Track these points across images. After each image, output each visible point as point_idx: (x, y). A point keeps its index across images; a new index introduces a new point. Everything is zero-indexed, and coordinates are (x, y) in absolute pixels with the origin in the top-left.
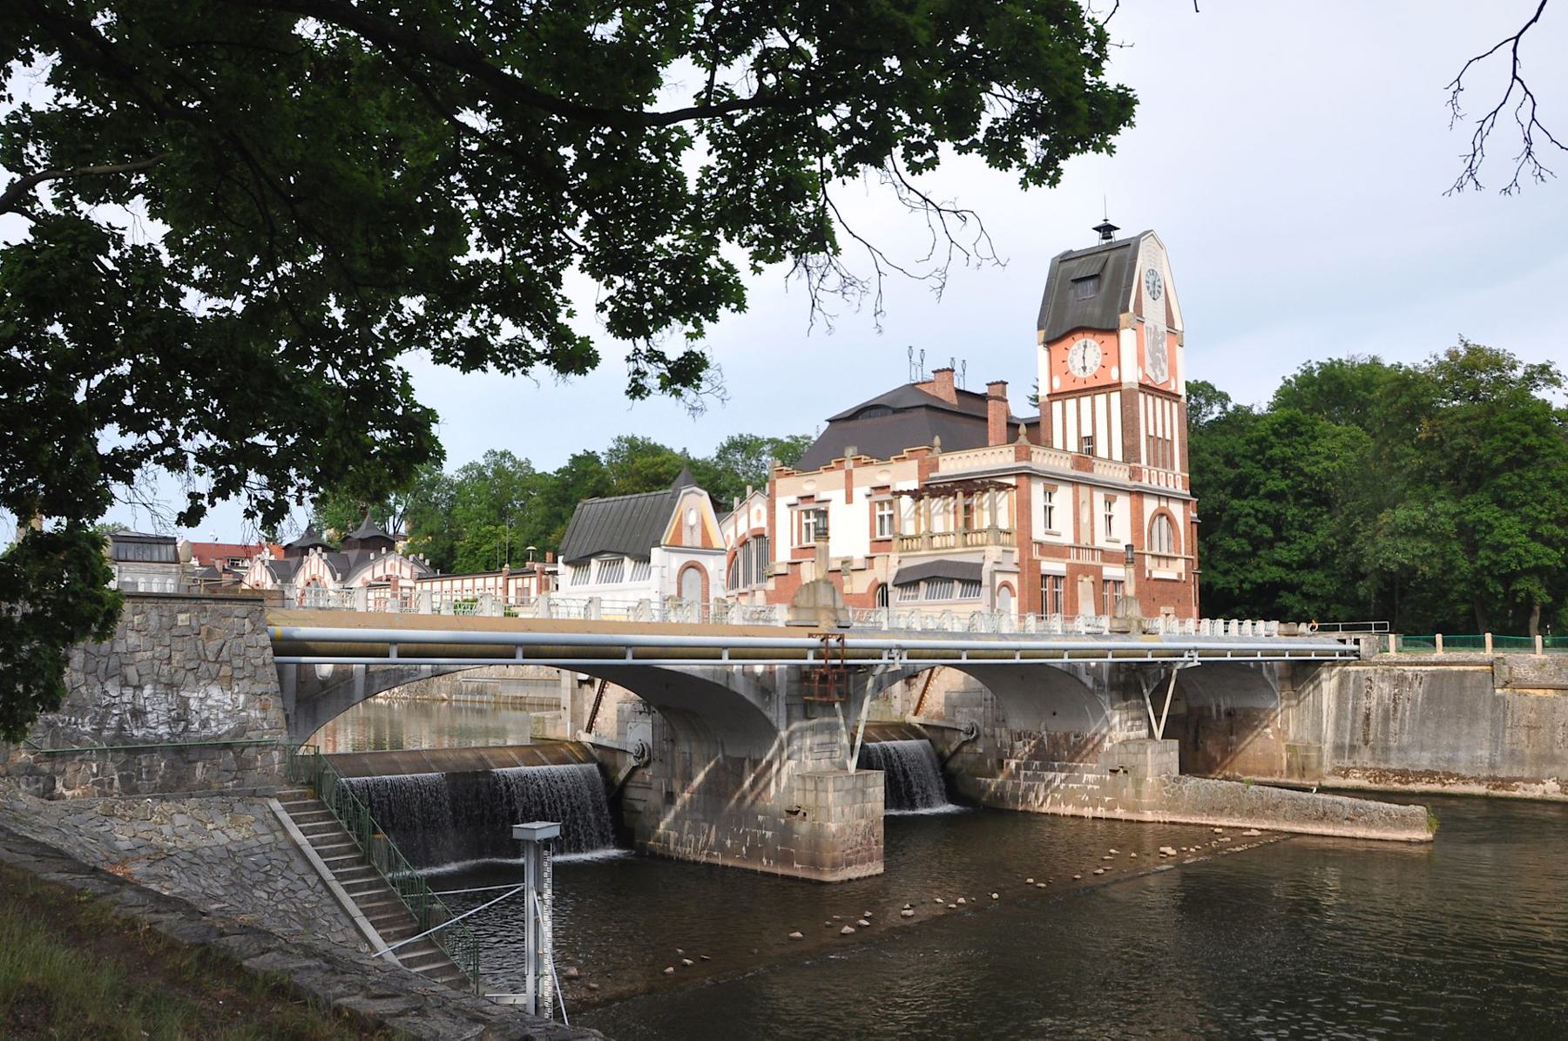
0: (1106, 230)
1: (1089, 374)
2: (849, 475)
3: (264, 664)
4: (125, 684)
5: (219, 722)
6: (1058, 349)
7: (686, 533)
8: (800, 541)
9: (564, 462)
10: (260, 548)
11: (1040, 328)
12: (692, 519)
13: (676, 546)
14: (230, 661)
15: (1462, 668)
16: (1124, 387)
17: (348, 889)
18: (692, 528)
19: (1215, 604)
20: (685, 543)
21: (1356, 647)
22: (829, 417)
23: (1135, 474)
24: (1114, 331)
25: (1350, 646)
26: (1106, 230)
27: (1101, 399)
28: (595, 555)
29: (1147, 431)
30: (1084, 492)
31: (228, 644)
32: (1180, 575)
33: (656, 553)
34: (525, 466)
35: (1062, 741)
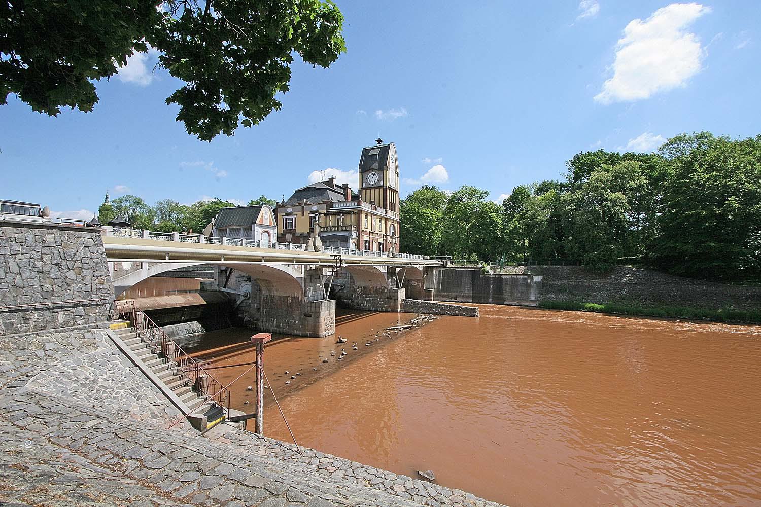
0: (379, 141)
2: (303, 207)
3: (101, 262)
6: (364, 175)
8: (286, 228)
17: (172, 389)
19: (403, 250)
26: (379, 141)
27: (377, 190)
31: (79, 251)
34: (177, 205)
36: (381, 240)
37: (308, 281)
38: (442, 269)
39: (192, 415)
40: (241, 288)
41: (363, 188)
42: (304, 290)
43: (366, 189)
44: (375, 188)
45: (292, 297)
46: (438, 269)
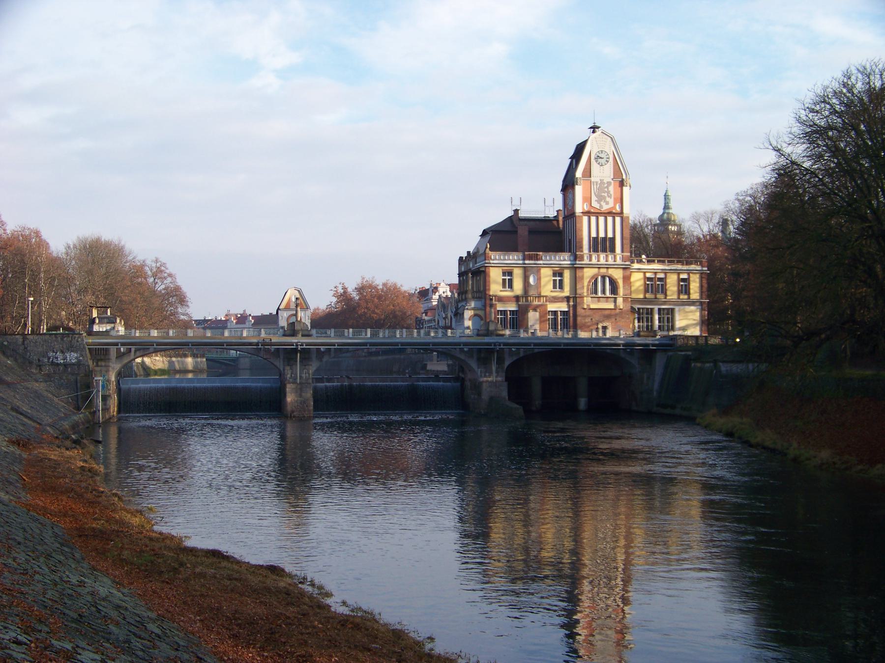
4: (54, 352)
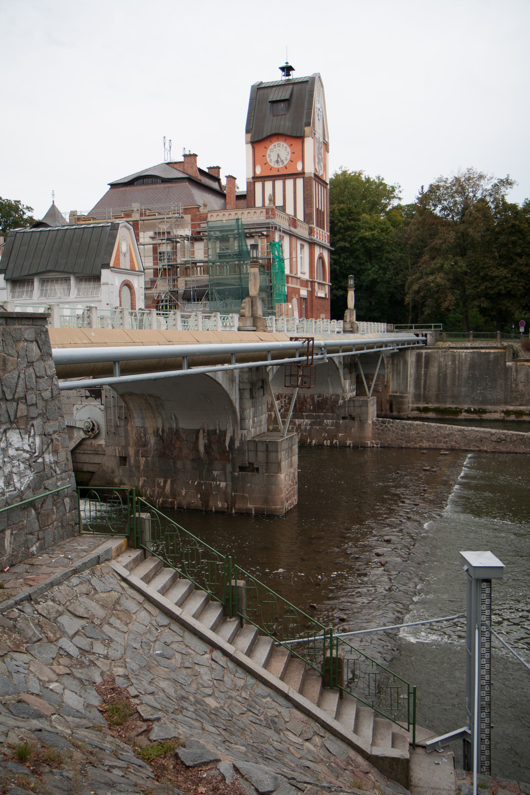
1: (281, 166)
5: (21, 475)
6: (260, 148)
7: (122, 257)
9: (373, 177)
10: (444, 262)
11: (247, 131)
12: (124, 248)
13: (117, 269)
14: (25, 398)
15: (487, 351)
16: (306, 176)
18: (125, 255)
20: (122, 266)
21: (424, 338)
22: (110, 182)
23: (311, 231)
24: (301, 138)
25: (420, 338)
26: (287, 69)
27: (289, 183)
28: (37, 274)
29: (316, 206)
30: (294, 239)
32: (326, 295)
33: (105, 274)
35: (309, 400)
36: (304, 293)
37: (247, 395)
38: (424, 351)
39: (377, 751)
40: (75, 412)
41: (256, 178)
42: (238, 415)
43: (263, 179)
44: (284, 177)
45: (208, 431)
46: (415, 352)
